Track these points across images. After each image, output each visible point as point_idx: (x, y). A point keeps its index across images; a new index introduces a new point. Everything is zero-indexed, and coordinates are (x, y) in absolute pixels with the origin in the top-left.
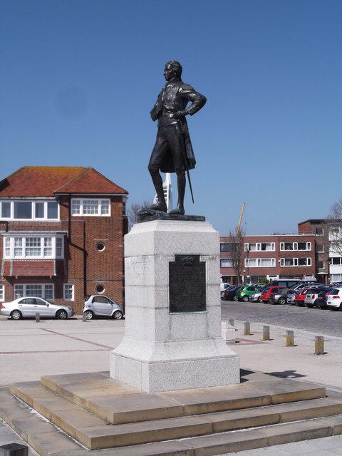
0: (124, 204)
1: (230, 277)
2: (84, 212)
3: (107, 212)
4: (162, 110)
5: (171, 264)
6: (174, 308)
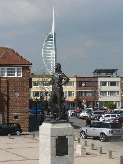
0: (30, 70)
1: (91, 102)
2: (8, 75)
3: (20, 75)
4: (54, 83)
5: (56, 139)
6: (57, 154)
